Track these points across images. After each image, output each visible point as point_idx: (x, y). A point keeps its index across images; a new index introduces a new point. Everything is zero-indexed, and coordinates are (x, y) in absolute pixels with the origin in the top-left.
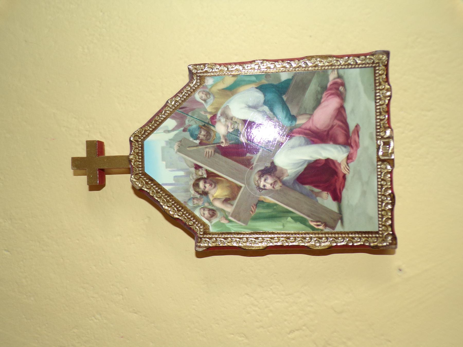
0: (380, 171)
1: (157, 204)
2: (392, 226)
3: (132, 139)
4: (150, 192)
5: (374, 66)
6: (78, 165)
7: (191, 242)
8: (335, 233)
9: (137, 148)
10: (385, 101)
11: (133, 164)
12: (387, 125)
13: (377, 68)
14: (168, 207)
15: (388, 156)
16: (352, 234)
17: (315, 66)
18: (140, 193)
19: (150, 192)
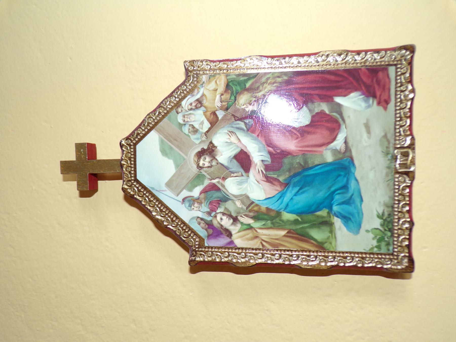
0: (397, 185)
3: (123, 143)
4: (139, 198)
6: (67, 168)
8: (381, 254)
9: (129, 153)
10: (406, 105)
11: (123, 170)
12: (408, 133)
13: (399, 66)
15: (406, 168)
17: (346, 63)
18: (130, 199)
19: (139, 198)
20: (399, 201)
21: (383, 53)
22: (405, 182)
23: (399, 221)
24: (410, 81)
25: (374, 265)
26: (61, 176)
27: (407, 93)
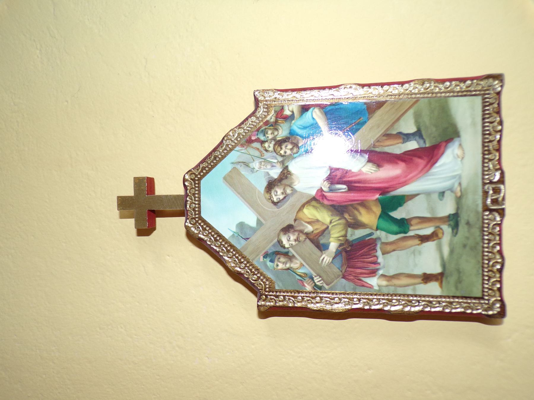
0: (487, 223)
1: (217, 254)
2: (500, 290)
3: (187, 177)
4: (206, 240)
5: (483, 94)
6: (124, 204)
7: (253, 299)
9: (193, 188)
10: (495, 137)
11: (183, 206)
14: (228, 257)
16: (432, 298)
20: (489, 240)
21: (469, 82)
22: (495, 219)
23: (489, 262)
24: (498, 112)
25: (462, 310)
26: (117, 212)
27: (495, 124)
